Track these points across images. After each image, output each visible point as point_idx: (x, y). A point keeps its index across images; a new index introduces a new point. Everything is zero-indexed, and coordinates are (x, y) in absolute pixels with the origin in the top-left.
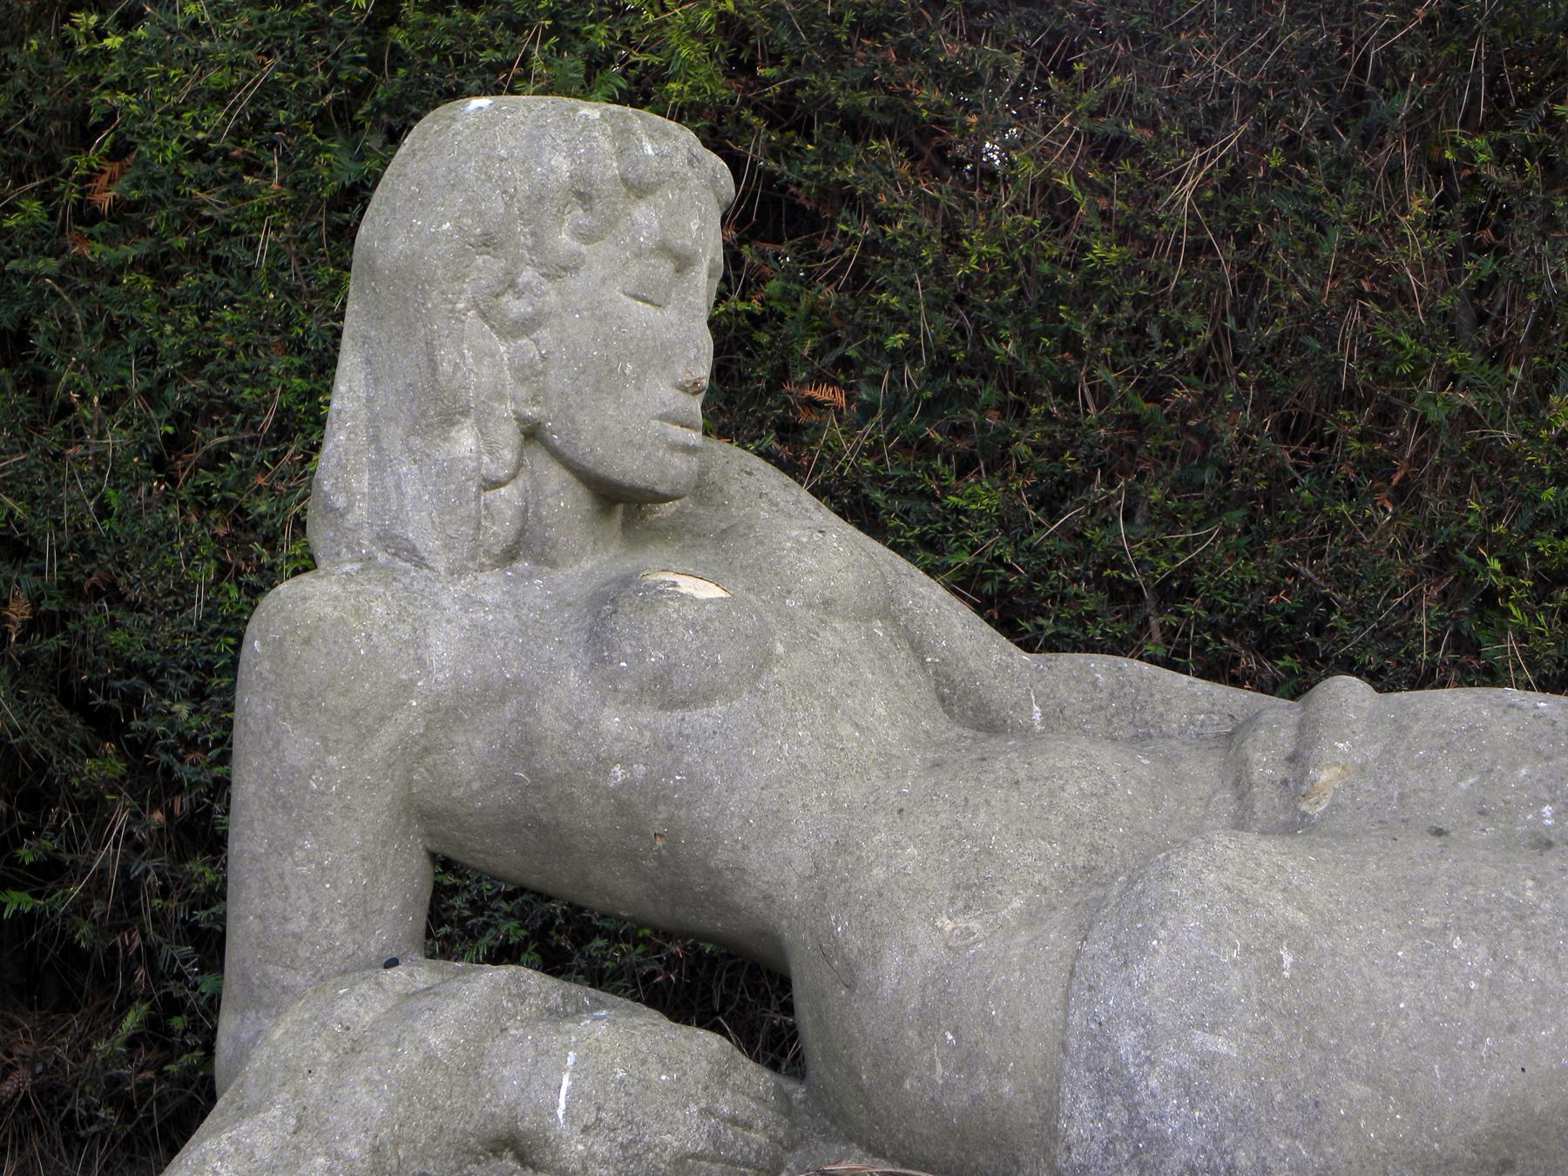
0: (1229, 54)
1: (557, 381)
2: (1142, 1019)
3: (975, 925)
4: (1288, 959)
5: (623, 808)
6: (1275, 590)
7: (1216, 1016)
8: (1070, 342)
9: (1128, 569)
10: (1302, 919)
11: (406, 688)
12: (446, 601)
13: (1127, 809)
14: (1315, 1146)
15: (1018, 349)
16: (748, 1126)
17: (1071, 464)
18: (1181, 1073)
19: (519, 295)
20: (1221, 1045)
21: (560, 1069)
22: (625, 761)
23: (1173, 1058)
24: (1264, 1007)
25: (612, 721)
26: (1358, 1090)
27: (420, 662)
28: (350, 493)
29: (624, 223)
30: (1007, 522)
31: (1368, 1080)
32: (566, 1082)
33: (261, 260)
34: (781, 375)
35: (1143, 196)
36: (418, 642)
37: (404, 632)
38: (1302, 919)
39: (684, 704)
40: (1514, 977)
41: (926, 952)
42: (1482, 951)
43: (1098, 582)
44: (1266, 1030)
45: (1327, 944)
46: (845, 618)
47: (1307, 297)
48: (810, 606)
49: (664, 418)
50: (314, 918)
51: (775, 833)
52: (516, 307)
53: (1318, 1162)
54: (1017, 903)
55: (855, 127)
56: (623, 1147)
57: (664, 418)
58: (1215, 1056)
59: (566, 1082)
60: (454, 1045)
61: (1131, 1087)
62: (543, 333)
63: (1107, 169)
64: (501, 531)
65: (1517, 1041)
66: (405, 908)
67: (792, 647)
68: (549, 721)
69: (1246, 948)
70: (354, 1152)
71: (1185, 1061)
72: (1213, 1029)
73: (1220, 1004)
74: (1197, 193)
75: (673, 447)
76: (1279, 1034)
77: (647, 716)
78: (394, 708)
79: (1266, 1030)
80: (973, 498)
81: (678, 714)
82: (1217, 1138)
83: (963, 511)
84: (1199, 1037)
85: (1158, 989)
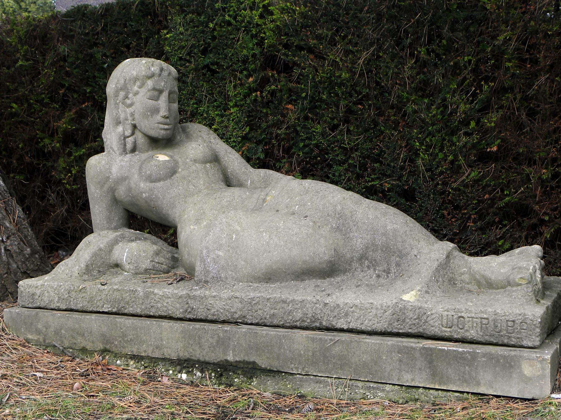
0: (373, 31)
1: (137, 116)
2: (207, 248)
3: (196, 227)
4: (234, 237)
5: (146, 202)
6: (374, 149)
7: (220, 248)
8: (337, 95)
9: (346, 145)
10: (239, 229)
11: (108, 177)
12: (117, 160)
13: (235, 204)
14: (236, 273)
15: (327, 97)
16: (162, 264)
17: (336, 122)
18: (213, 258)
19: (129, 99)
20: (220, 253)
21: (125, 252)
22: (145, 193)
23: (212, 256)
24: (229, 246)
25: (142, 185)
26: (243, 263)
27: (110, 172)
28: (107, 138)
29: (146, 84)
30: (323, 134)
31: (245, 261)
32: (126, 255)
33: (189, 80)
34: (280, 103)
35: (354, 63)
36: (110, 169)
37: (107, 167)
38: (239, 229)
39: (155, 182)
40: (272, 242)
41: (187, 233)
42: (268, 236)
43: (340, 147)
44: (229, 251)
45: (242, 234)
46: (199, 163)
47: (385, 84)
48: (191, 161)
49: (158, 123)
50: (100, 221)
51: (173, 207)
52: (128, 102)
53: (236, 276)
54: (205, 223)
55: (300, 48)
56: (136, 267)
57: (158, 123)
58: (219, 255)
59: (126, 255)
60: (106, 247)
61: (205, 261)
62: (133, 107)
63: (346, 57)
64: (129, 146)
65: (270, 254)
66: (119, 219)
67: (183, 170)
68: (133, 185)
69: (227, 234)
70: (83, 266)
71: (214, 256)
72: (219, 250)
73: (221, 245)
74: (364, 62)
75: (161, 129)
76: (231, 252)
77: (148, 184)
78: (107, 181)
79: (229, 251)
80: (317, 129)
81: (154, 184)
82: (219, 271)
83: (315, 132)
84: (217, 251)
85: (210, 242)
